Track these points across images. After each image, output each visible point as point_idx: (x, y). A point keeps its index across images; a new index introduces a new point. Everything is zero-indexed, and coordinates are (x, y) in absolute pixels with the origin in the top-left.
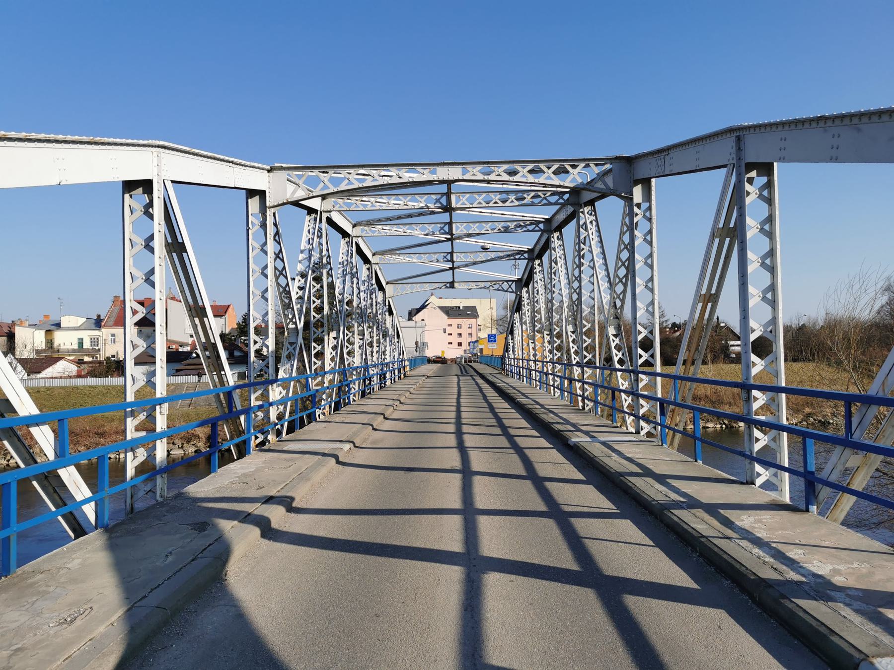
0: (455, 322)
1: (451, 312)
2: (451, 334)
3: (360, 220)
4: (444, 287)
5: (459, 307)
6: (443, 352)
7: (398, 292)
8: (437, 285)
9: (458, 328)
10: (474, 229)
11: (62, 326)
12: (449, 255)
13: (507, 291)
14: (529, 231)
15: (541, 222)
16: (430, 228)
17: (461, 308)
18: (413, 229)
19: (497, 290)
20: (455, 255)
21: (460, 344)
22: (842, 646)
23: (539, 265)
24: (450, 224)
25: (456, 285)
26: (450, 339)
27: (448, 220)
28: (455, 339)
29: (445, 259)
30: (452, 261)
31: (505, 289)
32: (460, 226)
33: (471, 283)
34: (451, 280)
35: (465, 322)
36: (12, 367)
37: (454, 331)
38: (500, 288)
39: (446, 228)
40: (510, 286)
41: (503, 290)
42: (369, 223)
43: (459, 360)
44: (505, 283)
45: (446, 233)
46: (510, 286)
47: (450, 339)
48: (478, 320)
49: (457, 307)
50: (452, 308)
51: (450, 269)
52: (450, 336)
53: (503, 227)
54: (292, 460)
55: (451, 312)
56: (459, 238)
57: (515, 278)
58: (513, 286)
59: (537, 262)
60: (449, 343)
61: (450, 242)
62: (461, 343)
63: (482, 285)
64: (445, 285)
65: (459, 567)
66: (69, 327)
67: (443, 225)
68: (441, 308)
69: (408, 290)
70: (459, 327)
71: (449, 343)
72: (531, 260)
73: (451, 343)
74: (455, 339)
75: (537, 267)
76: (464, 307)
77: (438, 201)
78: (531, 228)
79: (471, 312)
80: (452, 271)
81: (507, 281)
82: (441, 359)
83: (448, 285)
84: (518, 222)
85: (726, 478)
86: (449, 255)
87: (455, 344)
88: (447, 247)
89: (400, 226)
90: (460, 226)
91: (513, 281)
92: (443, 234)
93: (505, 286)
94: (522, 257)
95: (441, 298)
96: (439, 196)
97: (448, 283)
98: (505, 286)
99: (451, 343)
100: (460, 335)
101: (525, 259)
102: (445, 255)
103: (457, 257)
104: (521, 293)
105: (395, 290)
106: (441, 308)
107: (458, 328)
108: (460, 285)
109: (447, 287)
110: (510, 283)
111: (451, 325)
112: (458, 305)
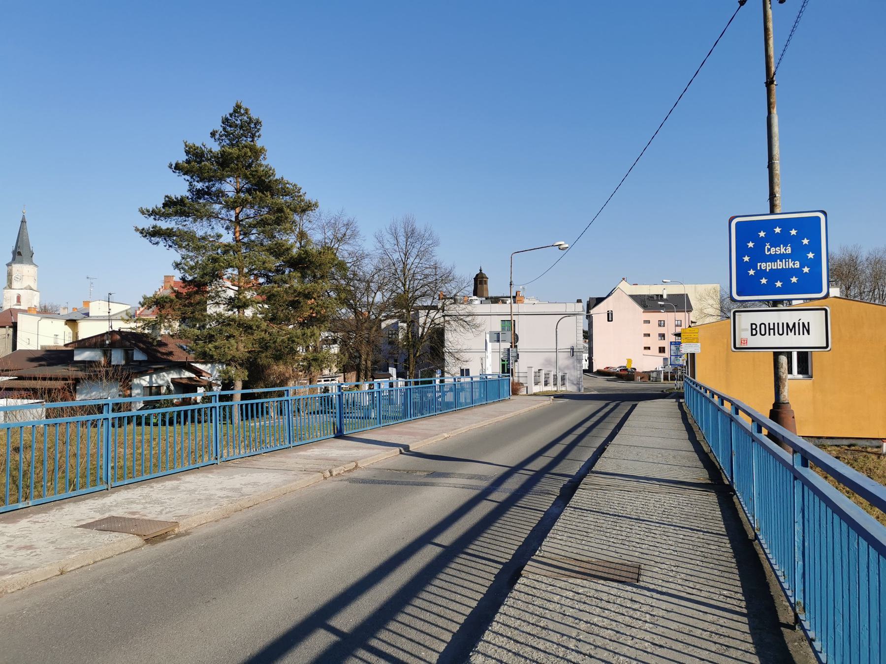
0: (654, 317)
1: (648, 303)
2: (649, 335)
5: (662, 296)
6: (629, 361)
9: (660, 325)
11: (90, 315)
17: (665, 297)
21: (662, 350)
22: (369, 655)
26: (647, 342)
28: (657, 343)
35: (670, 318)
36: (729, 401)
37: (655, 330)
43: (654, 375)
47: (647, 342)
48: (691, 314)
49: (657, 295)
50: (651, 297)
55: (648, 303)
60: (645, 348)
62: (660, 348)
65: (328, 623)
66: (97, 317)
68: (635, 298)
70: (661, 324)
71: (645, 348)
73: (649, 348)
74: (657, 343)
76: (668, 295)
79: (679, 303)
82: (626, 373)
85: (257, 387)
87: (655, 350)
99: (649, 348)
100: (662, 336)
106: (635, 298)
107: (660, 325)
112: (661, 293)
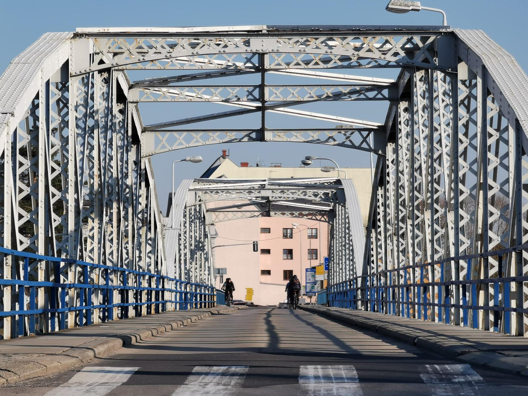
3: (138, 79)
4: (246, 139)
7: (164, 147)
8: (233, 135)
10: (293, 95)
12: (258, 89)
13: (359, 148)
14: (368, 99)
15: (383, 87)
16: (233, 92)
18: (212, 94)
19: (342, 145)
20: (267, 90)
23: (406, 110)
24: (262, 87)
25: (268, 135)
27: (259, 83)
29: (251, 97)
30: (262, 98)
31: (357, 144)
32: (276, 58)
33: (294, 133)
34: (259, 127)
38: (348, 143)
39: (256, 93)
40: (365, 140)
41: (353, 146)
42: (152, 84)
44: (357, 133)
45: (255, 100)
46: (365, 140)
47: (265, 262)
51: (258, 109)
52: (244, 161)
53: (331, 93)
54: (176, 342)
56: (272, 107)
57: (375, 124)
58: (371, 139)
59: (403, 105)
61: (260, 74)
63: (315, 135)
64: (248, 135)
67: (251, 55)
69: (181, 144)
72: (394, 101)
75: (403, 114)
77: (249, 60)
78: (371, 94)
80: (260, 113)
81: (360, 130)
83: (254, 135)
84: (353, 88)
86: (258, 89)
88: (256, 79)
89: (193, 88)
90: (276, 58)
91: (370, 130)
92: (252, 100)
93: (357, 139)
94: (379, 96)
95: (245, 165)
96: (252, 88)
97: (254, 131)
98: (357, 139)
99: (268, 272)
101: (384, 98)
102: (251, 89)
103: (271, 94)
104: (384, 152)
105: (157, 142)
108: (274, 136)
109: (251, 139)
110: (365, 133)
111: (266, 230)
